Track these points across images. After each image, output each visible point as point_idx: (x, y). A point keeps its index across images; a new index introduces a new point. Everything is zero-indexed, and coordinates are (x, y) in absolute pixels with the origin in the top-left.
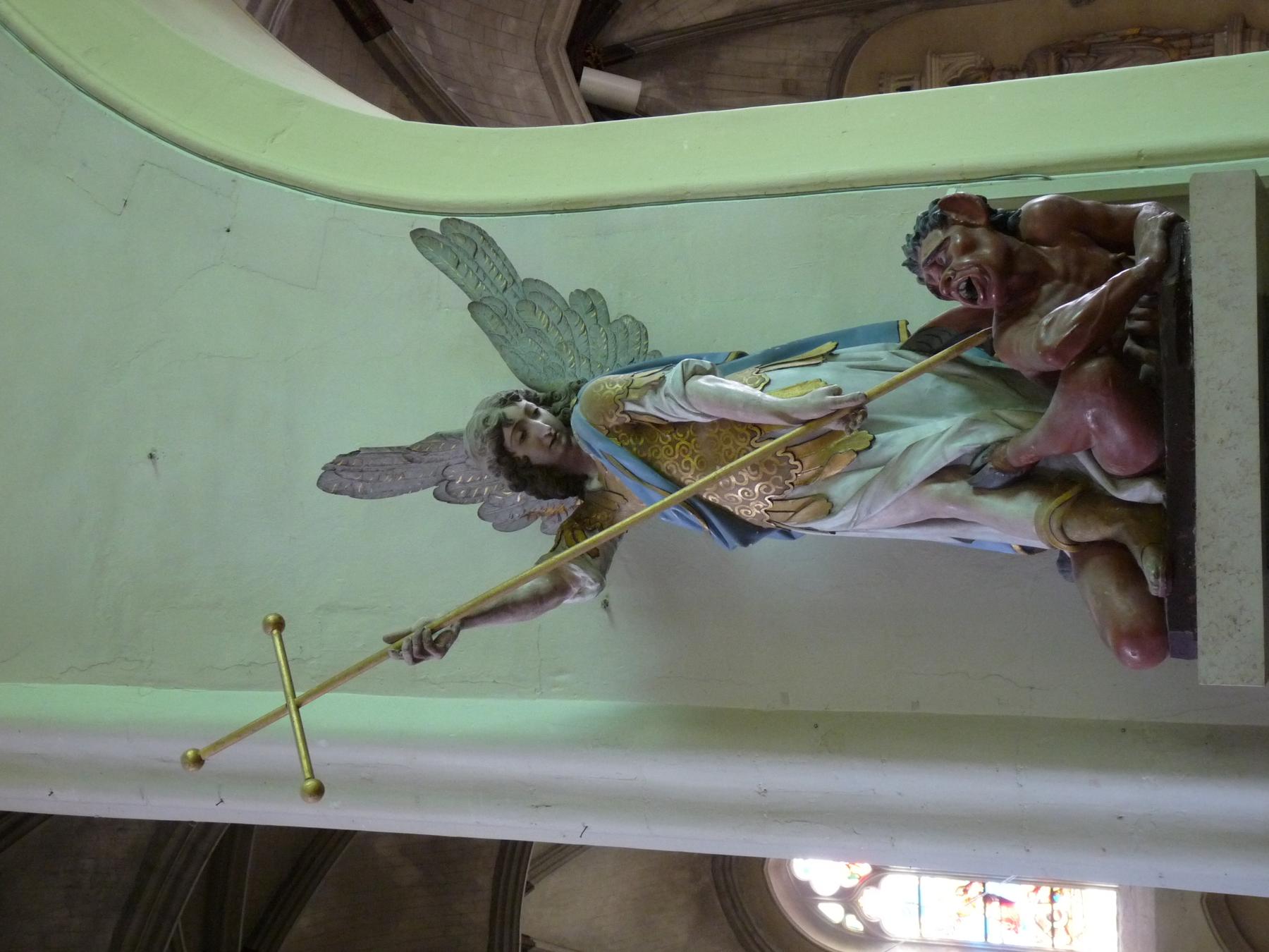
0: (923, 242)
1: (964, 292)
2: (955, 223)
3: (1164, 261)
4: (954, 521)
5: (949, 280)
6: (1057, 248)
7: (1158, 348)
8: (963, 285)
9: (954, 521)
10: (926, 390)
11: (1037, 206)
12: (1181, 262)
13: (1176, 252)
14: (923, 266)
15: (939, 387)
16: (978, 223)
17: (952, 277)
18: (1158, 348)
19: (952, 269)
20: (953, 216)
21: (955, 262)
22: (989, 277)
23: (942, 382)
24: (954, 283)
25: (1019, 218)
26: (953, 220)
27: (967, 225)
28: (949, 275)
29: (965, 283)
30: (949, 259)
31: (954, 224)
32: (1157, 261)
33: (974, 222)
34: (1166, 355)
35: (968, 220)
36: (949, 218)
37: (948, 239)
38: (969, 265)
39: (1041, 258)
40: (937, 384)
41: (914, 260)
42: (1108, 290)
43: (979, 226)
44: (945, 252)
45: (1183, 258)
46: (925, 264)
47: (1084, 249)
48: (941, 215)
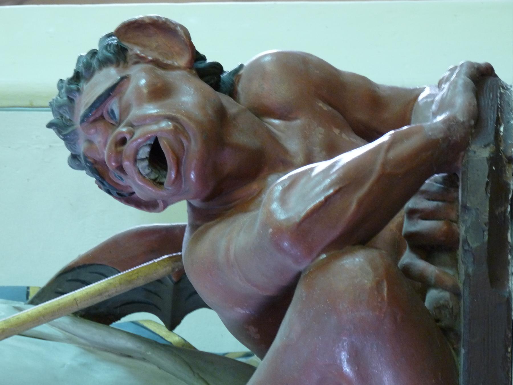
0: (85, 86)
1: (146, 163)
2: (140, 60)
3: (473, 122)
4: (113, 268)
5: (123, 141)
6: (298, 122)
7: (455, 265)
8: (144, 152)
9: (113, 268)
10: (63, 365)
11: (268, 59)
12: (497, 131)
13: (491, 116)
14: (82, 121)
15: (84, 365)
16: (176, 64)
17: (128, 137)
18: (455, 265)
19: (130, 125)
20: (137, 50)
21: (135, 112)
22: (188, 139)
23: (90, 359)
24: (129, 148)
25: (240, 76)
26: (137, 55)
27: (156, 63)
28: (122, 133)
29: (148, 149)
30: (125, 110)
31: (136, 63)
32: (461, 120)
33: (169, 62)
34: (470, 270)
35: (161, 59)
36: (130, 53)
37: (124, 79)
38: (156, 119)
39: (270, 134)
40: (83, 359)
41: (68, 117)
42: (386, 145)
43: (178, 68)
44: (120, 99)
45: (500, 125)
46: (85, 117)
47: (337, 131)
48: (117, 46)
